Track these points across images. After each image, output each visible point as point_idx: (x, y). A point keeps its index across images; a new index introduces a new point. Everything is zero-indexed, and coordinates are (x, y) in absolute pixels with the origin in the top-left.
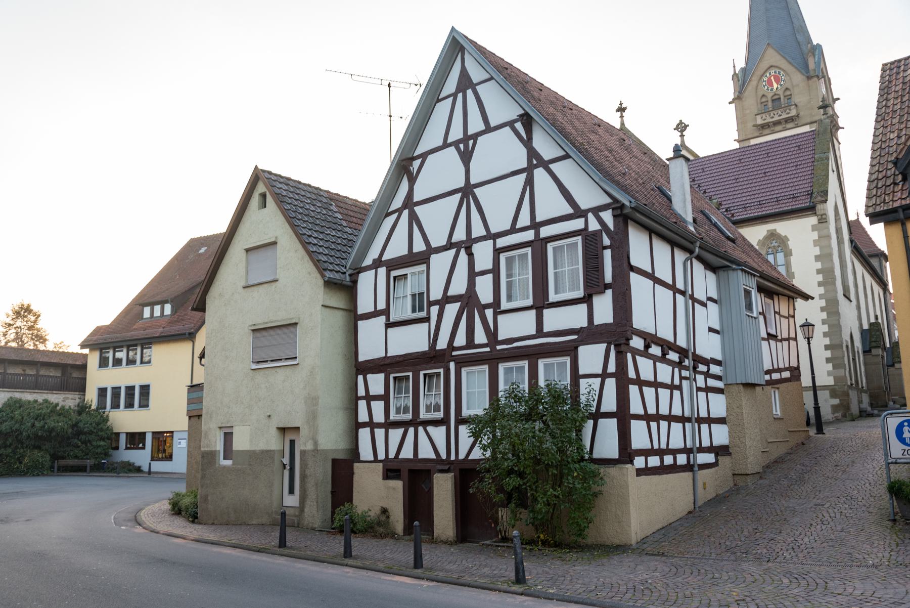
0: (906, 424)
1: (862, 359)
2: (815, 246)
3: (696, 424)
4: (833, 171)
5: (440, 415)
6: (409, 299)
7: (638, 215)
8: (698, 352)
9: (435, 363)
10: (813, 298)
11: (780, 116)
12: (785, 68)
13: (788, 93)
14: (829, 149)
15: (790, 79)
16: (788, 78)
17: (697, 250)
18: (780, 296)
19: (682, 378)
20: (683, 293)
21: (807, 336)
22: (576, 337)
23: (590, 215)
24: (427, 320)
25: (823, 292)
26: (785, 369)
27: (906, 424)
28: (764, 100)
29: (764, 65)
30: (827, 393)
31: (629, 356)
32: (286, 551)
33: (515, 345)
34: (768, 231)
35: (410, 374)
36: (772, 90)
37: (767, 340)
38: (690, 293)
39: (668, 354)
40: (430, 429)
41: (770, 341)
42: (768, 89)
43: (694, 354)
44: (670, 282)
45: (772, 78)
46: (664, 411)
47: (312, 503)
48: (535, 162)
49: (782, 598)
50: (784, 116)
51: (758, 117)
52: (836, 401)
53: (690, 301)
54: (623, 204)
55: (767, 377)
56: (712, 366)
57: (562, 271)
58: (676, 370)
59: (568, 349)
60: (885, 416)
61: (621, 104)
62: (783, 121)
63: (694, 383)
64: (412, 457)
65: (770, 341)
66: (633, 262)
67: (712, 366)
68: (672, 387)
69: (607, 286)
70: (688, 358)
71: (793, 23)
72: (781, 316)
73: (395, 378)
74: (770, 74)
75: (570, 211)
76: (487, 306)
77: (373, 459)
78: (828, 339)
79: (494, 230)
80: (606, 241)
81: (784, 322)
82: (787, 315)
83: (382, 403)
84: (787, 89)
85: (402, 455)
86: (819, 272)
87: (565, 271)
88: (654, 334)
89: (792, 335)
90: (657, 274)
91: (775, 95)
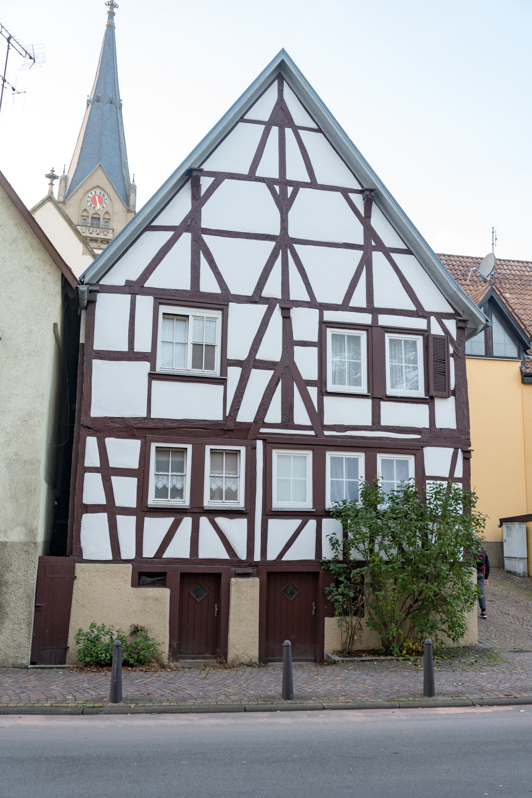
5: (240, 503)
6: (190, 347)
9: (229, 438)
12: (109, 194)
13: (107, 216)
15: (112, 205)
16: (110, 204)
23: (433, 319)
24: (222, 381)
28: (85, 214)
29: (92, 183)
32: (299, 703)
33: (349, 433)
35: (189, 447)
36: (94, 208)
40: (220, 521)
42: (91, 206)
45: (97, 197)
47: (16, 627)
48: (373, 244)
49: (180, 687)
50: (101, 236)
59: (415, 448)
61: (53, 171)
62: (100, 240)
64: (187, 556)
71: (121, 157)
73: (212, 452)
74: (95, 193)
76: (311, 383)
77: (110, 558)
79: (377, 304)
83: (133, 482)
84: (107, 212)
85: (169, 553)
91: (96, 213)
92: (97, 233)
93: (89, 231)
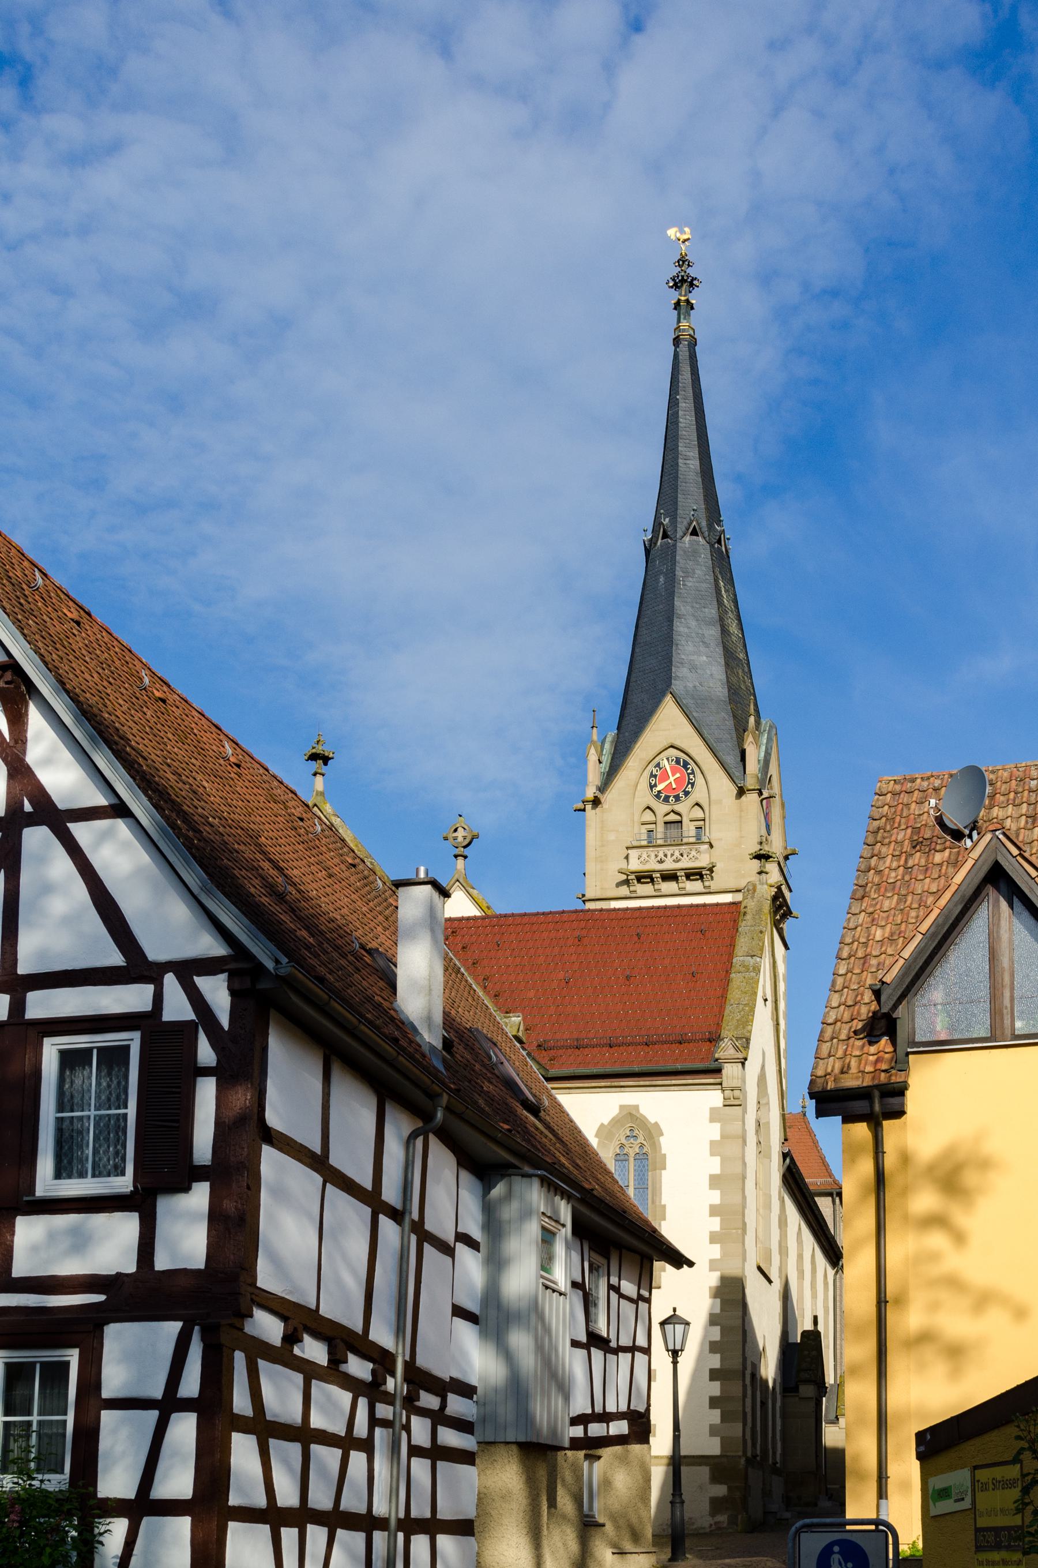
0: (836, 1549)
1: (778, 1404)
2: (712, 1154)
3: (400, 1536)
4: (766, 1000)
7: (294, 998)
8: (421, 1361)
10: (691, 1264)
11: (677, 861)
14: (762, 949)
17: (440, 1115)
18: (624, 1251)
19: (374, 1422)
20: (396, 1215)
21: (671, 1347)
22: (101, 1298)
25: (718, 1256)
26: (619, 1416)
27: (836, 1549)
30: (705, 1471)
31: (239, 1359)
34: (622, 1107)
37: (586, 1346)
38: (415, 1216)
39: (346, 1362)
41: (593, 1349)
43: (410, 1366)
44: (368, 1185)
46: (321, 1499)
50: (686, 863)
51: (634, 854)
52: (720, 1490)
53: (413, 1238)
54: (261, 966)
55: (578, 1431)
56: (452, 1398)
57: (81, 1118)
58: (363, 1403)
60: (798, 1531)
62: (682, 873)
63: (404, 1435)
65: (593, 1349)
66: (273, 1119)
67: (452, 1398)
68: (347, 1443)
69: (200, 1174)
70: (393, 1374)
72: (622, 1296)
75: (115, 958)
78: (718, 1356)
80: (206, 1053)
81: (627, 1308)
82: (635, 1296)
86: (714, 1211)
87: (89, 1117)
88: (313, 1307)
89: (641, 1342)
90: (337, 1159)
92: (674, 857)
93: (656, 856)
